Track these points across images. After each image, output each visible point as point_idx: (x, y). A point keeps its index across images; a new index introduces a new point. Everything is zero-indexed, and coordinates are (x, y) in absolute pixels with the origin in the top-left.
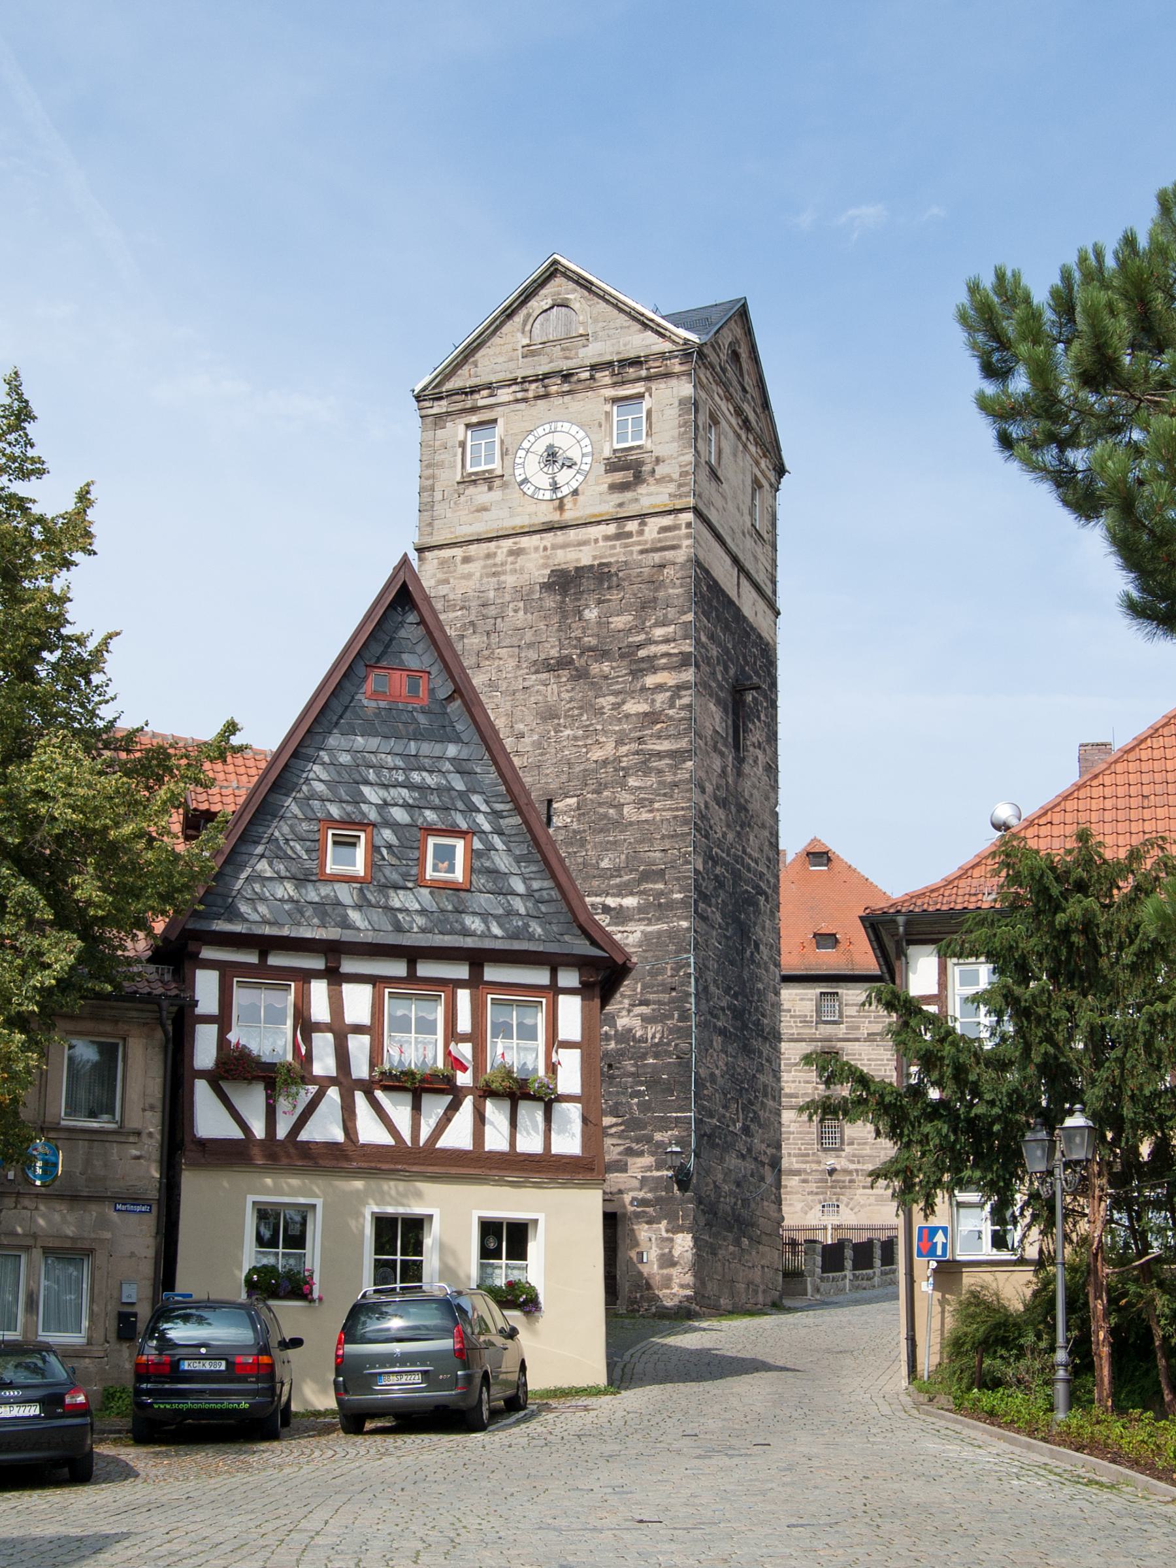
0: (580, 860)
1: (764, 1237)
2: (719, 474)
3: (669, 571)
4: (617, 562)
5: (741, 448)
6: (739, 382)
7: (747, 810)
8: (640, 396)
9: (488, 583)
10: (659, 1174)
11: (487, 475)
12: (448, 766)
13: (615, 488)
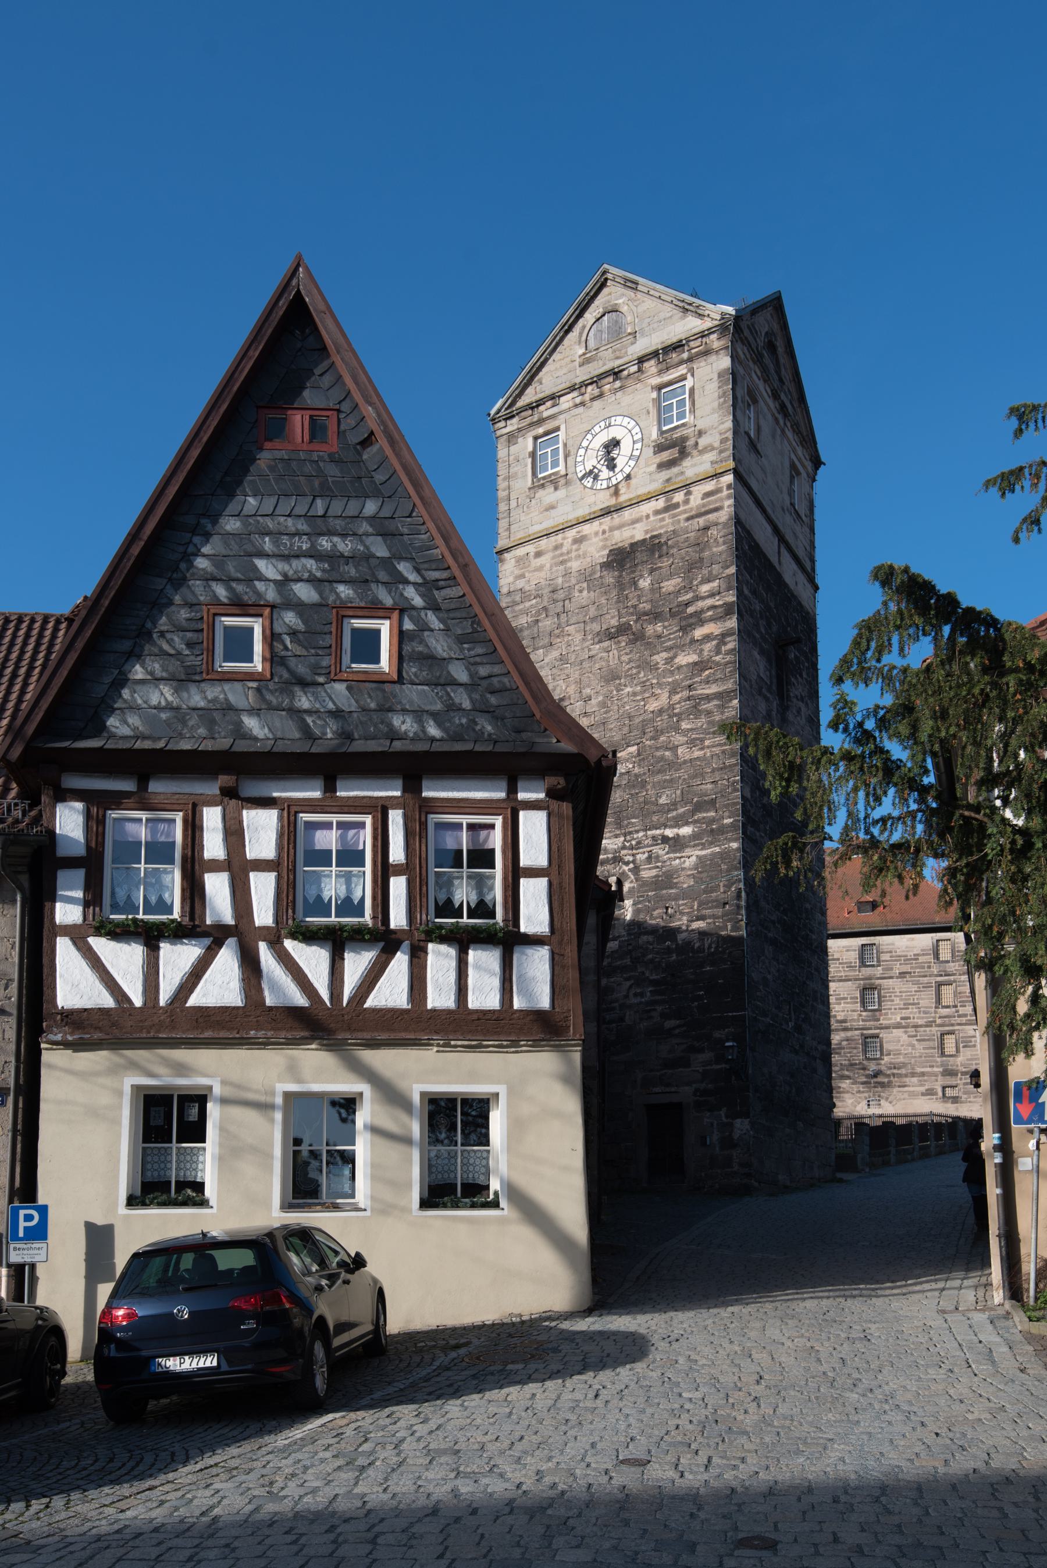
0: (641, 799)
2: (759, 447)
3: (713, 532)
4: (667, 532)
5: (779, 432)
6: (776, 372)
8: (683, 378)
9: (557, 571)
10: (719, 1067)
11: (553, 477)
12: (365, 527)
13: (662, 466)
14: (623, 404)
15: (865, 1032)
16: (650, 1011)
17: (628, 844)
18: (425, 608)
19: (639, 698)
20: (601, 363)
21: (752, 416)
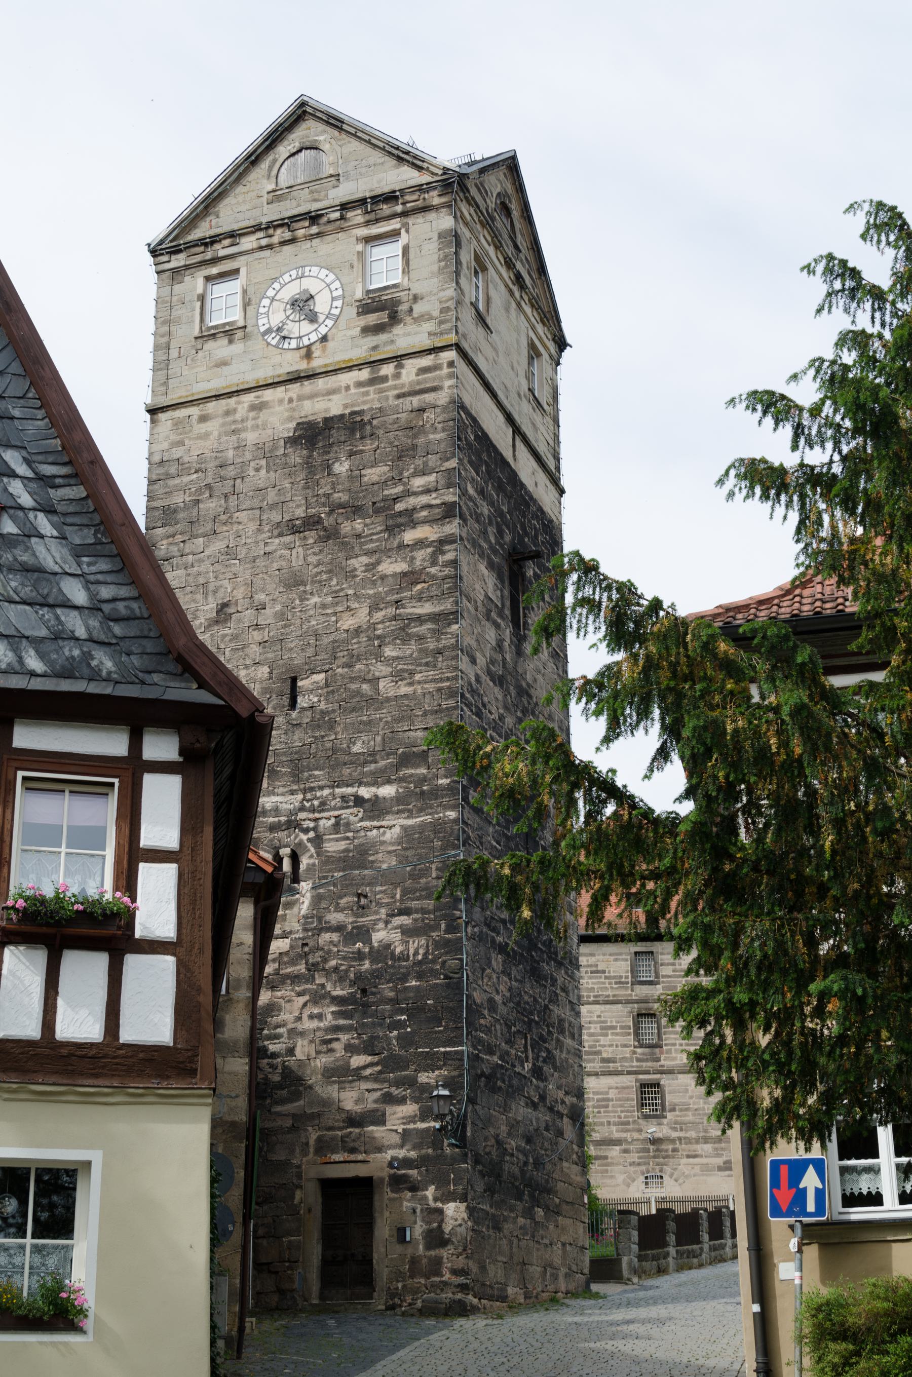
0: (329, 745)
1: (564, 1206)
3: (429, 415)
4: (371, 409)
5: (514, 305)
6: (511, 237)
7: (530, 697)
8: (395, 234)
10: (424, 1125)
11: (228, 328)
13: (367, 330)
14: (321, 253)
15: (641, 1077)
16: (330, 1041)
17: (307, 805)
18: (34, 509)
19: (329, 611)
20: (294, 203)
21: (480, 284)
